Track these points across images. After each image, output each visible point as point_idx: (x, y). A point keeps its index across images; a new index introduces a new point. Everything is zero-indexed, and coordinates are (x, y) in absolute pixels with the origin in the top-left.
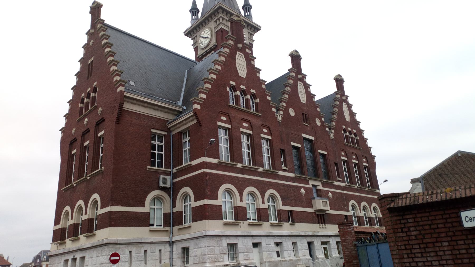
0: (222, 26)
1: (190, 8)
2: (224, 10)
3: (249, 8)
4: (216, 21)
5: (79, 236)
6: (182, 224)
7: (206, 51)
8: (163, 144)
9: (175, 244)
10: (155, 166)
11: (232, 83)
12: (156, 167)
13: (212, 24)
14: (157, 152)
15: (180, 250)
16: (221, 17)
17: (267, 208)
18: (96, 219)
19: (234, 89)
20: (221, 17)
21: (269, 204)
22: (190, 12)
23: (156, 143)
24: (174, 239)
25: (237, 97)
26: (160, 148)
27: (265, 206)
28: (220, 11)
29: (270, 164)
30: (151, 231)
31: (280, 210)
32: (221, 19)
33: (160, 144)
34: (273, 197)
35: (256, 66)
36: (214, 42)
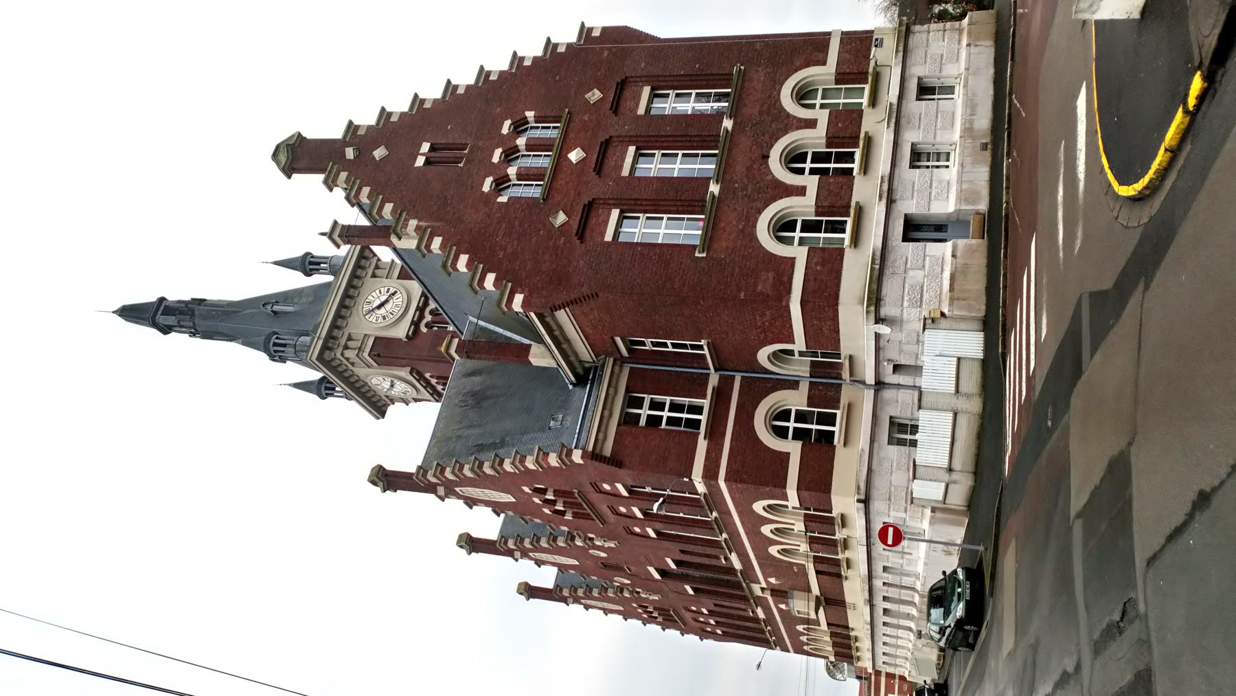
0: (366, 355)
2: (325, 347)
4: (353, 364)
5: (834, 514)
8: (648, 398)
9: (882, 379)
11: (486, 187)
12: (703, 418)
14: (666, 414)
16: (342, 354)
17: (827, 111)
18: (807, 509)
19: (502, 182)
20: (342, 354)
21: (818, 106)
23: (645, 412)
24: (870, 378)
25: (523, 175)
26: (659, 406)
27: (823, 117)
29: (703, 155)
30: (845, 444)
32: (348, 353)
33: (646, 404)
34: (803, 95)
35: (438, 95)
36: (404, 373)
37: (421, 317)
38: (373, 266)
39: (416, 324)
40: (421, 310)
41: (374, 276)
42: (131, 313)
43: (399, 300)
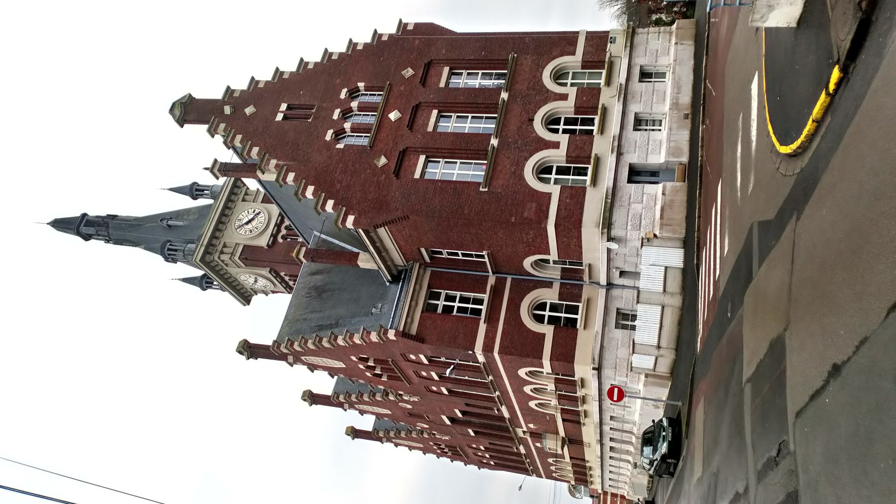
0: (237, 258)
1: (198, 289)
2: (206, 252)
3: (197, 190)
4: (227, 265)
6: (583, 270)
7: (272, 235)
8: (443, 293)
10: (481, 310)
13: (233, 270)
14: (456, 304)
15: (621, 279)
16: (219, 258)
19: (339, 134)
20: (219, 258)
21: (569, 85)
22: (204, 290)
23: (441, 303)
24: (603, 281)
26: (452, 299)
27: (572, 92)
28: (208, 258)
30: (585, 328)
31: (583, 61)
32: (223, 257)
33: (443, 297)
34: (559, 76)
37: (279, 231)
38: (243, 193)
39: (274, 236)
40: (278, 226)
41: (244, 200)
42: (61, 225)
43: (262, 218)
